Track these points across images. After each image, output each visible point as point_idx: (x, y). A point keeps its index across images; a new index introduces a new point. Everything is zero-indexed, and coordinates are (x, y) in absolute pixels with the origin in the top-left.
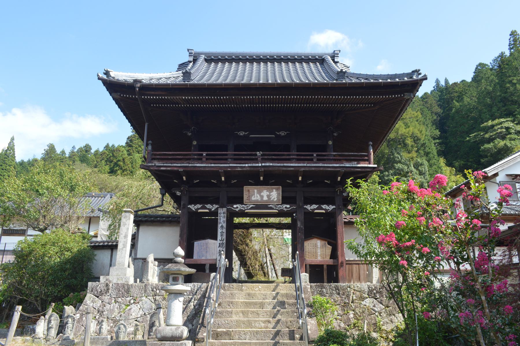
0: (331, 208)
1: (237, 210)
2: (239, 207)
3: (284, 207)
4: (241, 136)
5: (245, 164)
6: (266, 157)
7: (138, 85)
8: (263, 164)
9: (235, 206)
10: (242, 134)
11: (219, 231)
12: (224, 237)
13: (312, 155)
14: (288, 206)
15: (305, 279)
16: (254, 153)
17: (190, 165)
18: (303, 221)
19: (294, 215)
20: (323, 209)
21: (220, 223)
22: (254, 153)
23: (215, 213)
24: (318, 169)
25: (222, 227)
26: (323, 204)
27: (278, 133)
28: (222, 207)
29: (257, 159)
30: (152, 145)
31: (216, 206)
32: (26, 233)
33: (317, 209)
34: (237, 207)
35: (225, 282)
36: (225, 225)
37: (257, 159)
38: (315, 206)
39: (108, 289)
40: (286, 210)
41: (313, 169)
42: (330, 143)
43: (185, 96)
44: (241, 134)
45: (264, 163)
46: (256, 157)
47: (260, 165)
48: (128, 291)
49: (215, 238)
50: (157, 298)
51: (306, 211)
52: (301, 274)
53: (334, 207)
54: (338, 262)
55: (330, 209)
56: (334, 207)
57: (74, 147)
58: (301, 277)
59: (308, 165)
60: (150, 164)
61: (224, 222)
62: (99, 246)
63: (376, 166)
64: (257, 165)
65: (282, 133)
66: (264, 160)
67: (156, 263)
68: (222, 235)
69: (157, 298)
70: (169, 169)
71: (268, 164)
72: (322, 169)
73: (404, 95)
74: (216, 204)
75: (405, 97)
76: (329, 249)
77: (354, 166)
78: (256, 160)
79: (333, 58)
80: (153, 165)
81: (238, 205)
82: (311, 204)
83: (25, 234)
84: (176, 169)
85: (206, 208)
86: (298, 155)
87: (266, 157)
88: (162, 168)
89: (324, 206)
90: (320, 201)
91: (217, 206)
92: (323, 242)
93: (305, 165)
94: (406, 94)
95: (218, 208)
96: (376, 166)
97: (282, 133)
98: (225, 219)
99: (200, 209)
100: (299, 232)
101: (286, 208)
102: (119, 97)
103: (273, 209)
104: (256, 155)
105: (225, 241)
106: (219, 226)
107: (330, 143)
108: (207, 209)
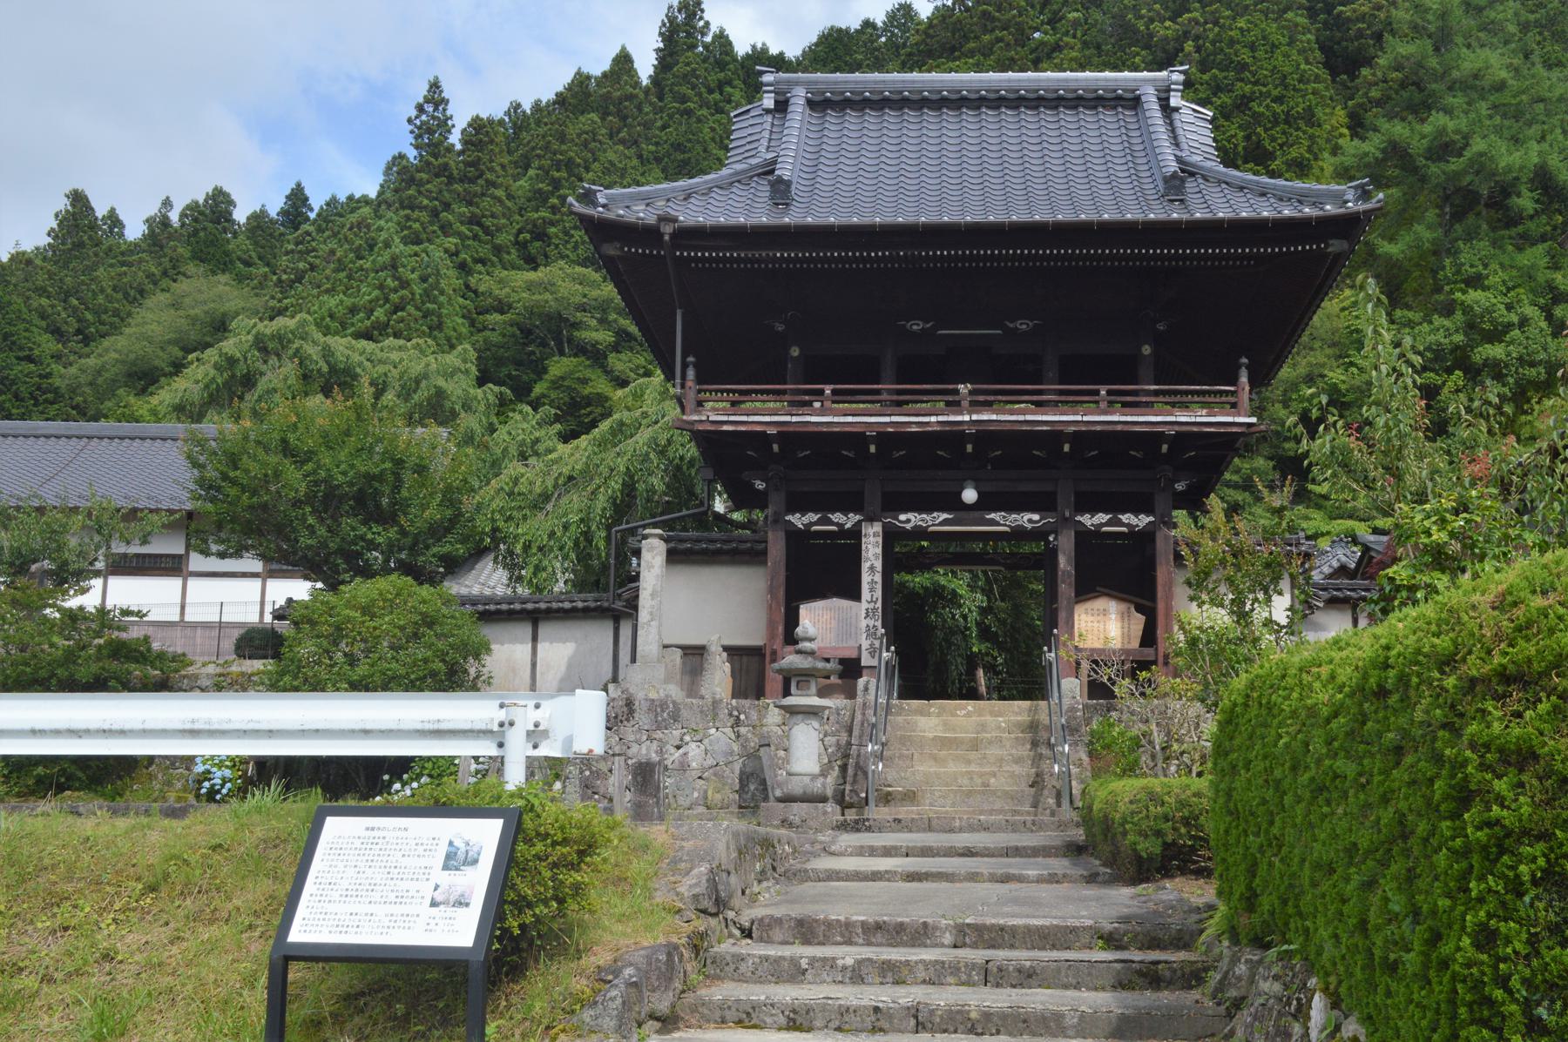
0: (1142, 521)
1: (908, 526)
2: (913, 519)
3: (1025, 518)
4: (914, 333)
5: (930, 415)
6: (981, 398)
7: (667, 229)
8: (975, 417)
9: (903, 517)
10: (916, 326)
11: (866, 578)
12: (879, 593)
13: (1097, 393)
14: (1036, 517)
15: (1072, 691)
16: (951, 387)
17: (794, 419)
18: (1073, 554)
19: (1051, 539)
20: (1123, 525)
21: (868, 559)
22: (951, 387)
23: (856, 534)
24: (1110, 428)
25: (872, 568)
26: (1124, 512)
27: (1011, 325)
28: (871, 519)
29: (958, 404)
30: (695, 366)
31: (854, 518)
32: (184, 568)
33: (1108, 524)
34: (908, 521)
35: (901, 697)
36: (879, 565)
37: (958, 404)
38: (1102, 518)
39: (631, 712)
40: (1029, 526)
41: (1098, 428)
42: (1147, 350)
43: (782, 250)
44: (915, 327)
45: (977, 412)
46: (957, 398)
47: (967, 418)
48: (675, 717)
49: (855, 595)
50: (743, 730)
51: (1080, 529)
52: (1063, 682)
53: (1151, 519)
54: (1157, 655)
55: (1141, 525)
56: (1151, 519)
57: (167, 203)
58: (1063, 686)
59: (1086, 418)
60: (696, 418)
61: (877, 558)
62: (499, 612)
63: (1254, 420)
64: (959, 418)
65: (1023, 325)
66: (976, 405)
67: (725, 654)
68: (872, 590)
69: (743, 730)
70: (743, 428)
71: (985, 417)
72: (1119, 428)
73: (1327, 246)
74: (856, 512)
75: (1329, 250)
76: (1139, 621)
77: (1199, 419)
78: (954, 405)
79: (1163, 95)
80: (704, 418)
81: (910, 516)
82: (1093, 511)
83: (181, 570)
84: (758, 428)
85: (831, 523)
86: (1061, 393)
87: (981, 398)
88: (725, 428)
89: (1127, 516)
90: (1115, 505)
91: (858, 517)
92: (1123, 606)
93: (1079, 418)
94: (1331, 242)
95: (860, 522)
96: (1254, 420)
97: (1023, 325)
98: (879, 550)
99: (816, 523)
100: (1064, 582)
101: (1030, 521)
102: (619, 253)
103: (998, 524)
104: (956, 392)
105: (879, 604)
106: (865, 566)
107: (1147, 350)
108: (832, 523)
